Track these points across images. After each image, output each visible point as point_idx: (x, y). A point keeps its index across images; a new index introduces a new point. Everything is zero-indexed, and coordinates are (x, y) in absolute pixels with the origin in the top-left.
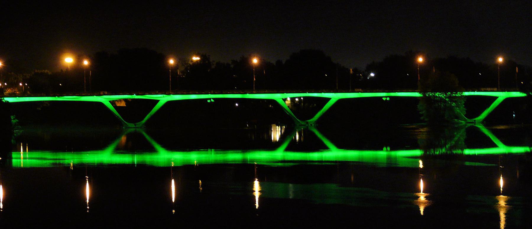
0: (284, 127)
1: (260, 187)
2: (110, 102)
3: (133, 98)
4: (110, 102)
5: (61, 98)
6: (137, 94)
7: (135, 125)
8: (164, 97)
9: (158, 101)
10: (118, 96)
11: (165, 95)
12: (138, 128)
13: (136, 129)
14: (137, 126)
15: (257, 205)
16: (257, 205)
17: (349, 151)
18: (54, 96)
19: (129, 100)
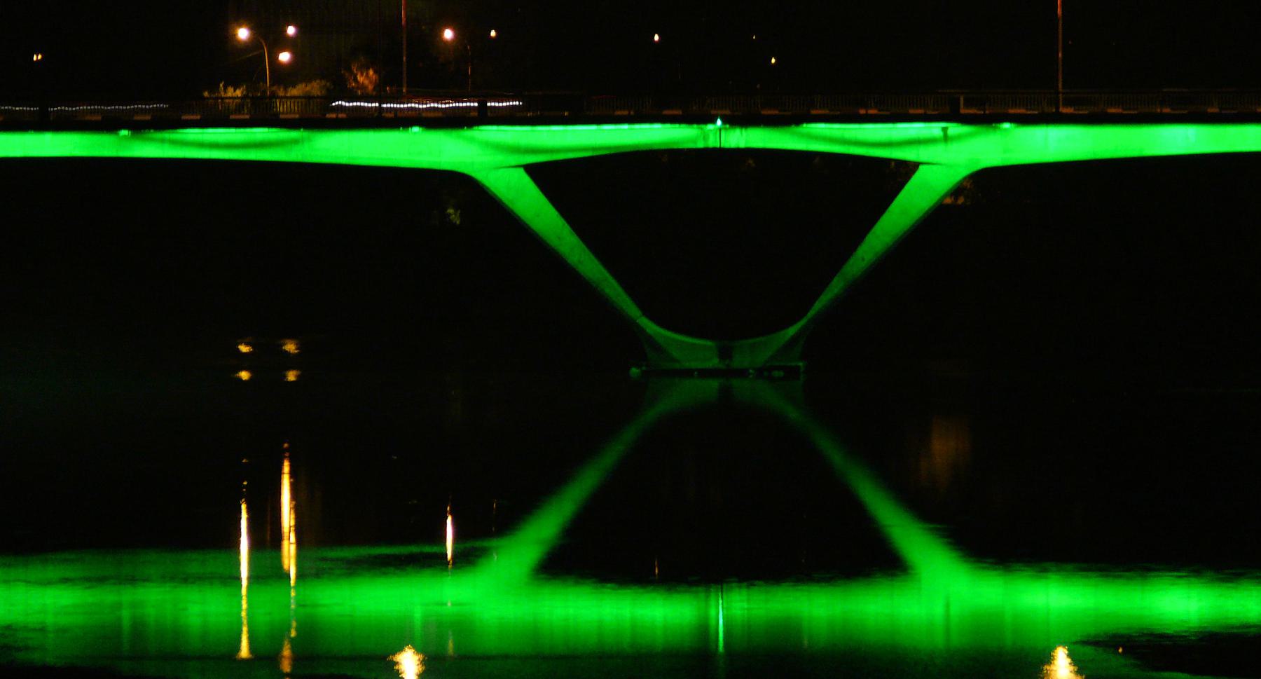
0: (206, 94)
1: (1072, 668)
2: (532, 170)
3: (713, 143)
4: (532, 170)
5: (163, 141)
6: (736, 120)
7: (725, 353)
8: (946, 138)
9: (907, 169)
10: (593, 128)
11: (954, 128)
12: (742, 373)
13: (736, 383)
14: (739, 361)
15: (244, 507)
16: (244, 507)
17: (519, 215)
18: (107, 125)
19: (949, 201)
